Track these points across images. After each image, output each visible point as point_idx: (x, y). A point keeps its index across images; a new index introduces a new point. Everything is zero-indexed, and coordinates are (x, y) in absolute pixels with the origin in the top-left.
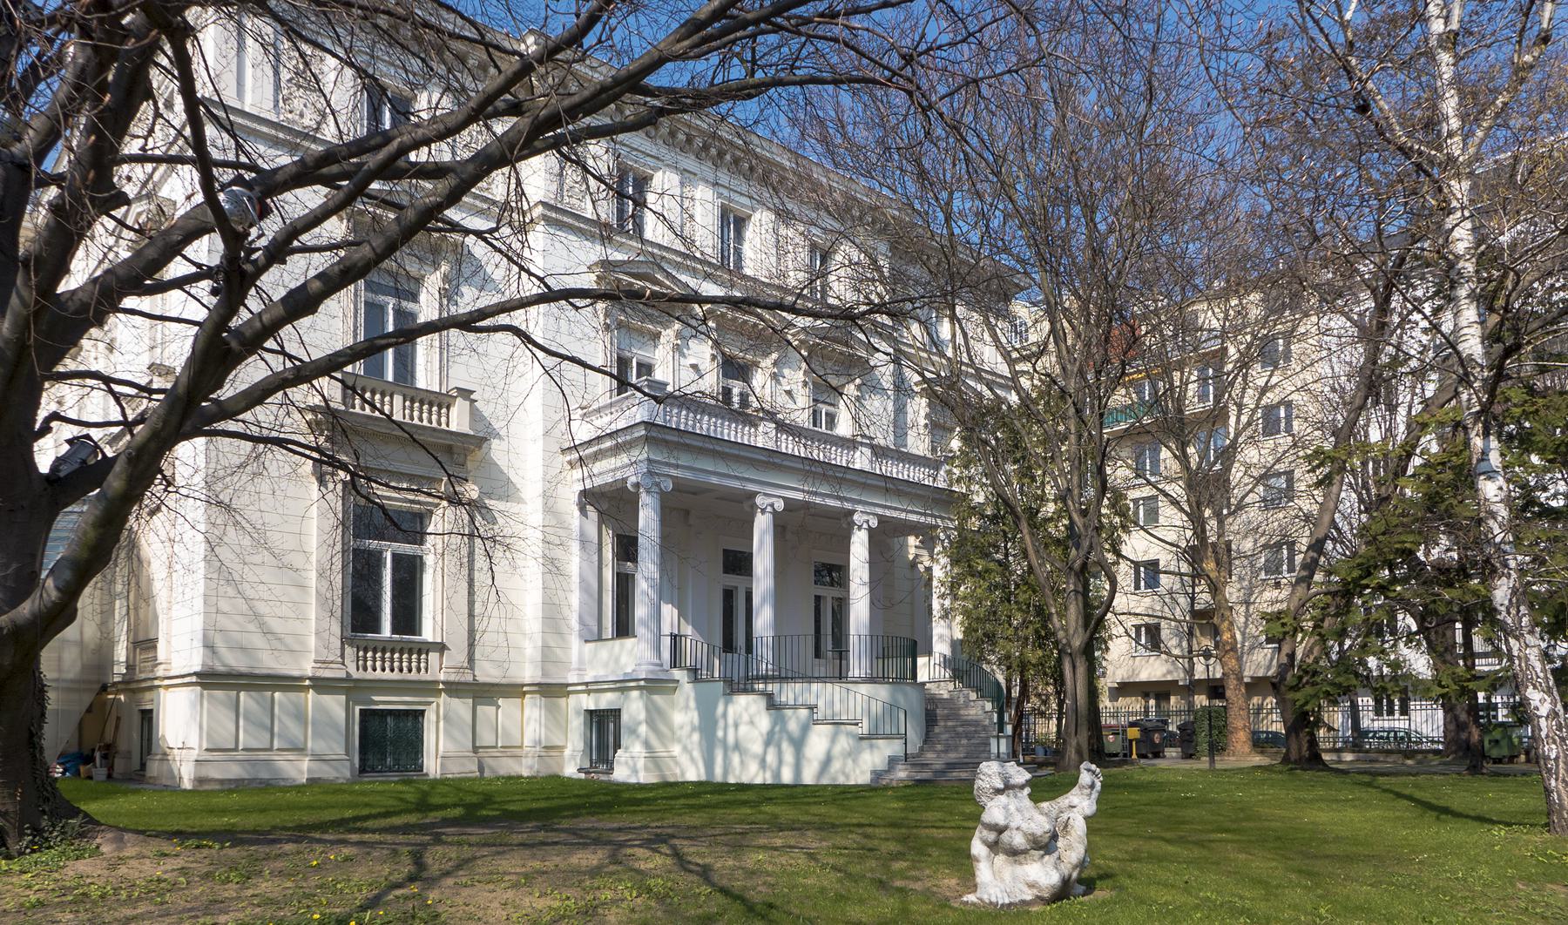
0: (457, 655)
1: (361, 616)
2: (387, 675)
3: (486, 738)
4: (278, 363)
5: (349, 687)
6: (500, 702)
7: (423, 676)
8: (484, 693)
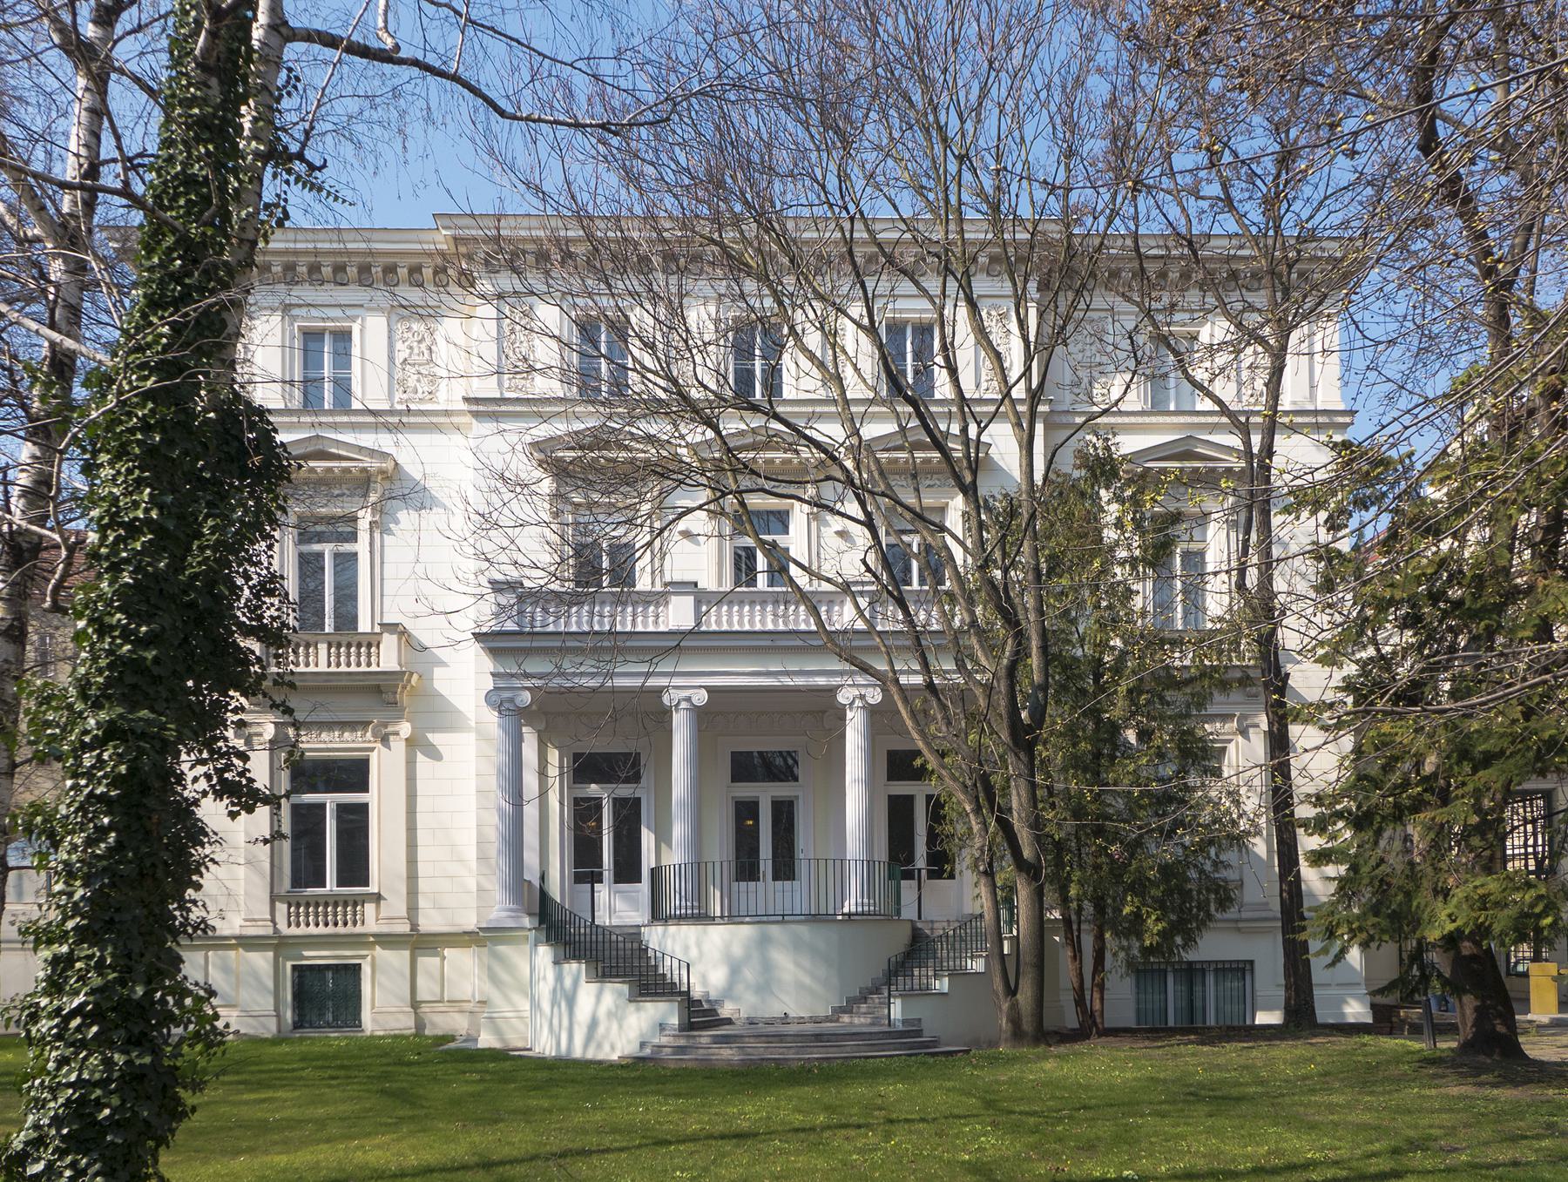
0: (396, 904)
1: (307, 870)
2: (312, 930)
3: (426, 989)
4: (815, 582)
5: (279, 944)
6: (447, 952)
7: (359, 929)
8: (420, 943)
